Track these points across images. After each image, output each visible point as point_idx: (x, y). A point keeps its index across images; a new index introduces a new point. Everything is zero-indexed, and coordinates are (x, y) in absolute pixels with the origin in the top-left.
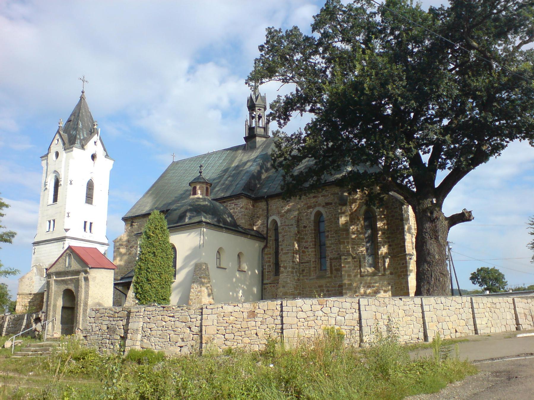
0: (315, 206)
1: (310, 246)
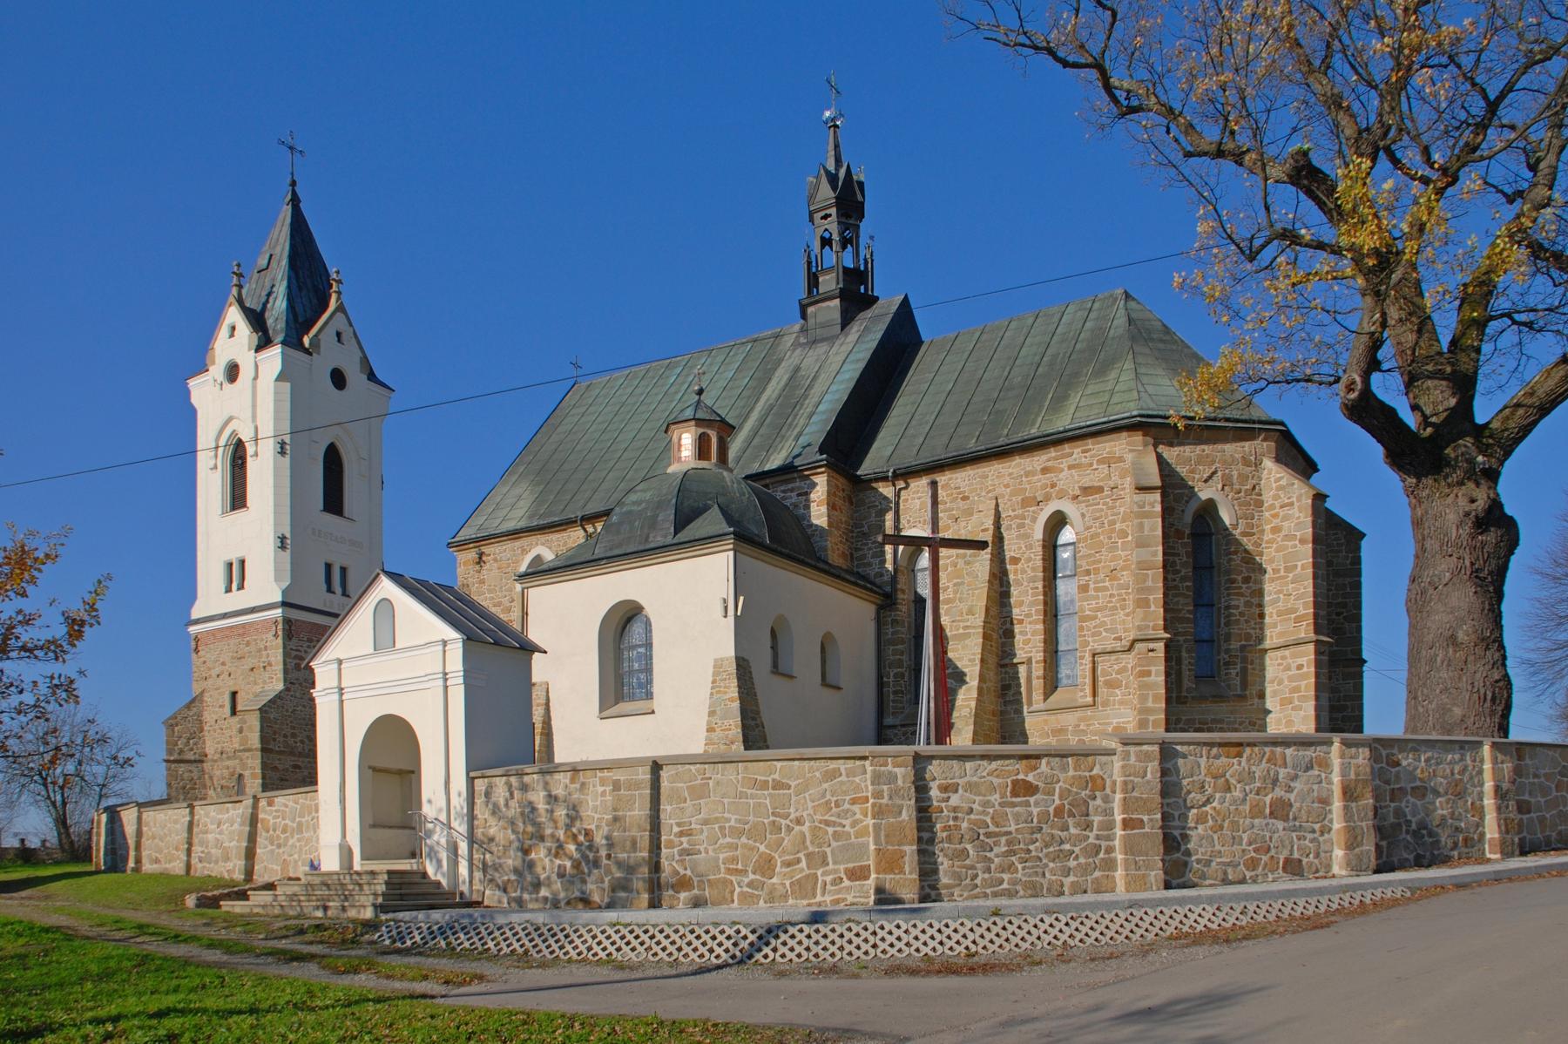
0: (1048, 498)
1: (1028, 616)
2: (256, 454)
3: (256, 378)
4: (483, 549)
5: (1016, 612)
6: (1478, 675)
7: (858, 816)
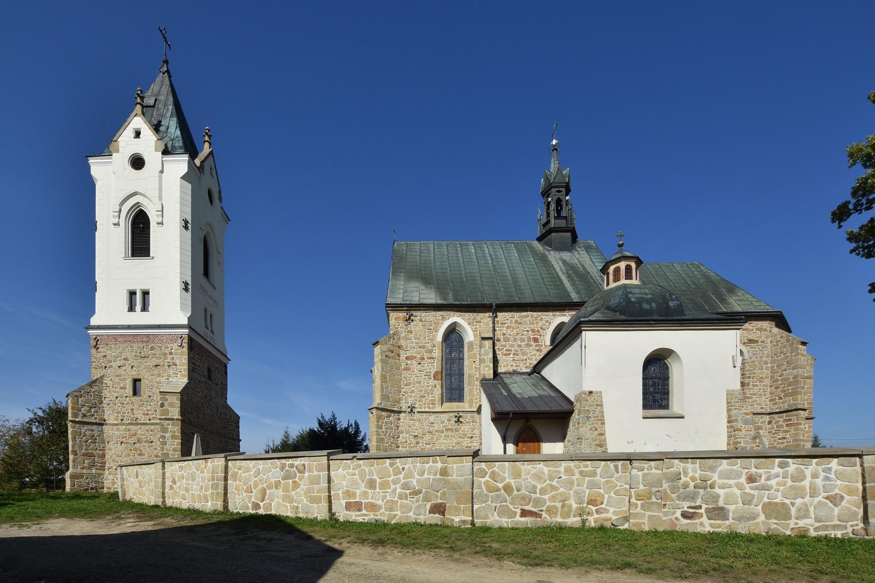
3: (162, 172)
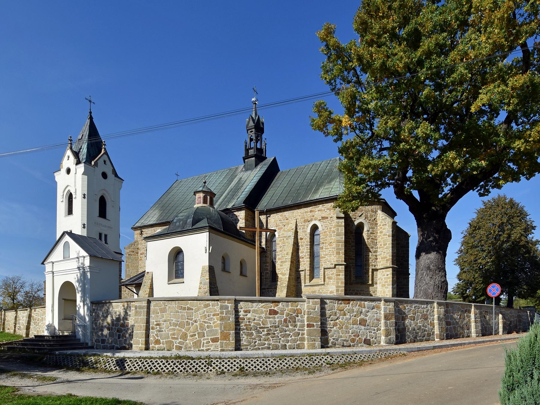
0: (312, 220)
2: (75, 198)
3: (76, 173)
4: (143, 230)
5: (301, 255)
6: (437, 280)
7: (216, 320)
